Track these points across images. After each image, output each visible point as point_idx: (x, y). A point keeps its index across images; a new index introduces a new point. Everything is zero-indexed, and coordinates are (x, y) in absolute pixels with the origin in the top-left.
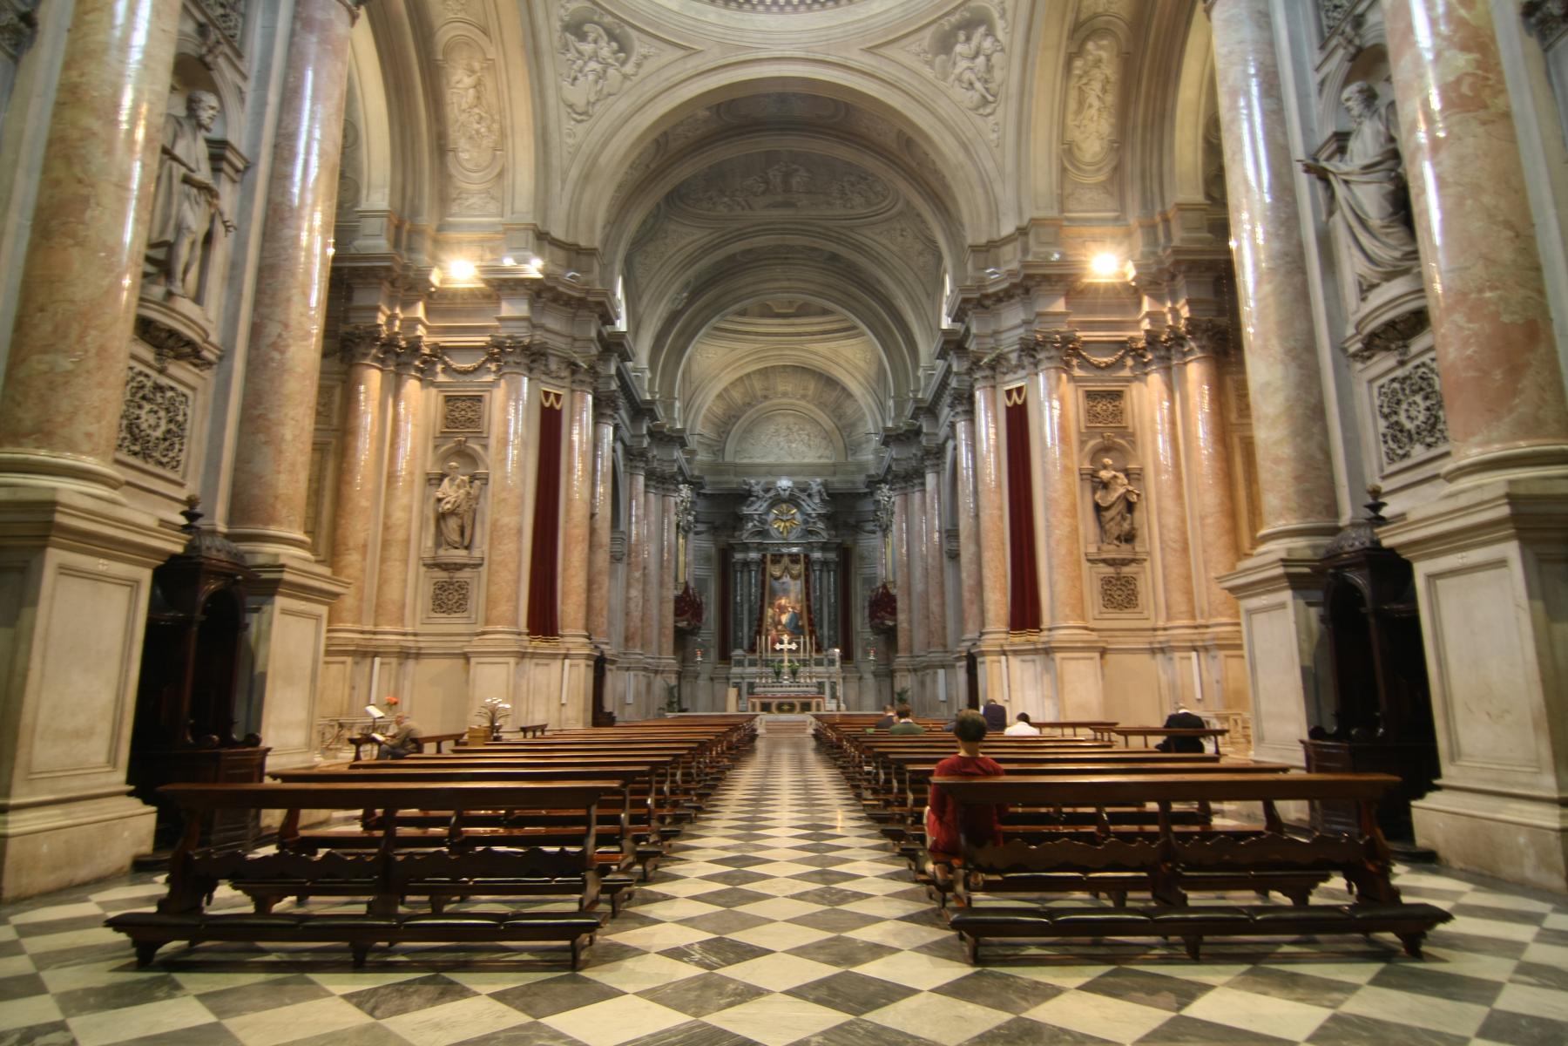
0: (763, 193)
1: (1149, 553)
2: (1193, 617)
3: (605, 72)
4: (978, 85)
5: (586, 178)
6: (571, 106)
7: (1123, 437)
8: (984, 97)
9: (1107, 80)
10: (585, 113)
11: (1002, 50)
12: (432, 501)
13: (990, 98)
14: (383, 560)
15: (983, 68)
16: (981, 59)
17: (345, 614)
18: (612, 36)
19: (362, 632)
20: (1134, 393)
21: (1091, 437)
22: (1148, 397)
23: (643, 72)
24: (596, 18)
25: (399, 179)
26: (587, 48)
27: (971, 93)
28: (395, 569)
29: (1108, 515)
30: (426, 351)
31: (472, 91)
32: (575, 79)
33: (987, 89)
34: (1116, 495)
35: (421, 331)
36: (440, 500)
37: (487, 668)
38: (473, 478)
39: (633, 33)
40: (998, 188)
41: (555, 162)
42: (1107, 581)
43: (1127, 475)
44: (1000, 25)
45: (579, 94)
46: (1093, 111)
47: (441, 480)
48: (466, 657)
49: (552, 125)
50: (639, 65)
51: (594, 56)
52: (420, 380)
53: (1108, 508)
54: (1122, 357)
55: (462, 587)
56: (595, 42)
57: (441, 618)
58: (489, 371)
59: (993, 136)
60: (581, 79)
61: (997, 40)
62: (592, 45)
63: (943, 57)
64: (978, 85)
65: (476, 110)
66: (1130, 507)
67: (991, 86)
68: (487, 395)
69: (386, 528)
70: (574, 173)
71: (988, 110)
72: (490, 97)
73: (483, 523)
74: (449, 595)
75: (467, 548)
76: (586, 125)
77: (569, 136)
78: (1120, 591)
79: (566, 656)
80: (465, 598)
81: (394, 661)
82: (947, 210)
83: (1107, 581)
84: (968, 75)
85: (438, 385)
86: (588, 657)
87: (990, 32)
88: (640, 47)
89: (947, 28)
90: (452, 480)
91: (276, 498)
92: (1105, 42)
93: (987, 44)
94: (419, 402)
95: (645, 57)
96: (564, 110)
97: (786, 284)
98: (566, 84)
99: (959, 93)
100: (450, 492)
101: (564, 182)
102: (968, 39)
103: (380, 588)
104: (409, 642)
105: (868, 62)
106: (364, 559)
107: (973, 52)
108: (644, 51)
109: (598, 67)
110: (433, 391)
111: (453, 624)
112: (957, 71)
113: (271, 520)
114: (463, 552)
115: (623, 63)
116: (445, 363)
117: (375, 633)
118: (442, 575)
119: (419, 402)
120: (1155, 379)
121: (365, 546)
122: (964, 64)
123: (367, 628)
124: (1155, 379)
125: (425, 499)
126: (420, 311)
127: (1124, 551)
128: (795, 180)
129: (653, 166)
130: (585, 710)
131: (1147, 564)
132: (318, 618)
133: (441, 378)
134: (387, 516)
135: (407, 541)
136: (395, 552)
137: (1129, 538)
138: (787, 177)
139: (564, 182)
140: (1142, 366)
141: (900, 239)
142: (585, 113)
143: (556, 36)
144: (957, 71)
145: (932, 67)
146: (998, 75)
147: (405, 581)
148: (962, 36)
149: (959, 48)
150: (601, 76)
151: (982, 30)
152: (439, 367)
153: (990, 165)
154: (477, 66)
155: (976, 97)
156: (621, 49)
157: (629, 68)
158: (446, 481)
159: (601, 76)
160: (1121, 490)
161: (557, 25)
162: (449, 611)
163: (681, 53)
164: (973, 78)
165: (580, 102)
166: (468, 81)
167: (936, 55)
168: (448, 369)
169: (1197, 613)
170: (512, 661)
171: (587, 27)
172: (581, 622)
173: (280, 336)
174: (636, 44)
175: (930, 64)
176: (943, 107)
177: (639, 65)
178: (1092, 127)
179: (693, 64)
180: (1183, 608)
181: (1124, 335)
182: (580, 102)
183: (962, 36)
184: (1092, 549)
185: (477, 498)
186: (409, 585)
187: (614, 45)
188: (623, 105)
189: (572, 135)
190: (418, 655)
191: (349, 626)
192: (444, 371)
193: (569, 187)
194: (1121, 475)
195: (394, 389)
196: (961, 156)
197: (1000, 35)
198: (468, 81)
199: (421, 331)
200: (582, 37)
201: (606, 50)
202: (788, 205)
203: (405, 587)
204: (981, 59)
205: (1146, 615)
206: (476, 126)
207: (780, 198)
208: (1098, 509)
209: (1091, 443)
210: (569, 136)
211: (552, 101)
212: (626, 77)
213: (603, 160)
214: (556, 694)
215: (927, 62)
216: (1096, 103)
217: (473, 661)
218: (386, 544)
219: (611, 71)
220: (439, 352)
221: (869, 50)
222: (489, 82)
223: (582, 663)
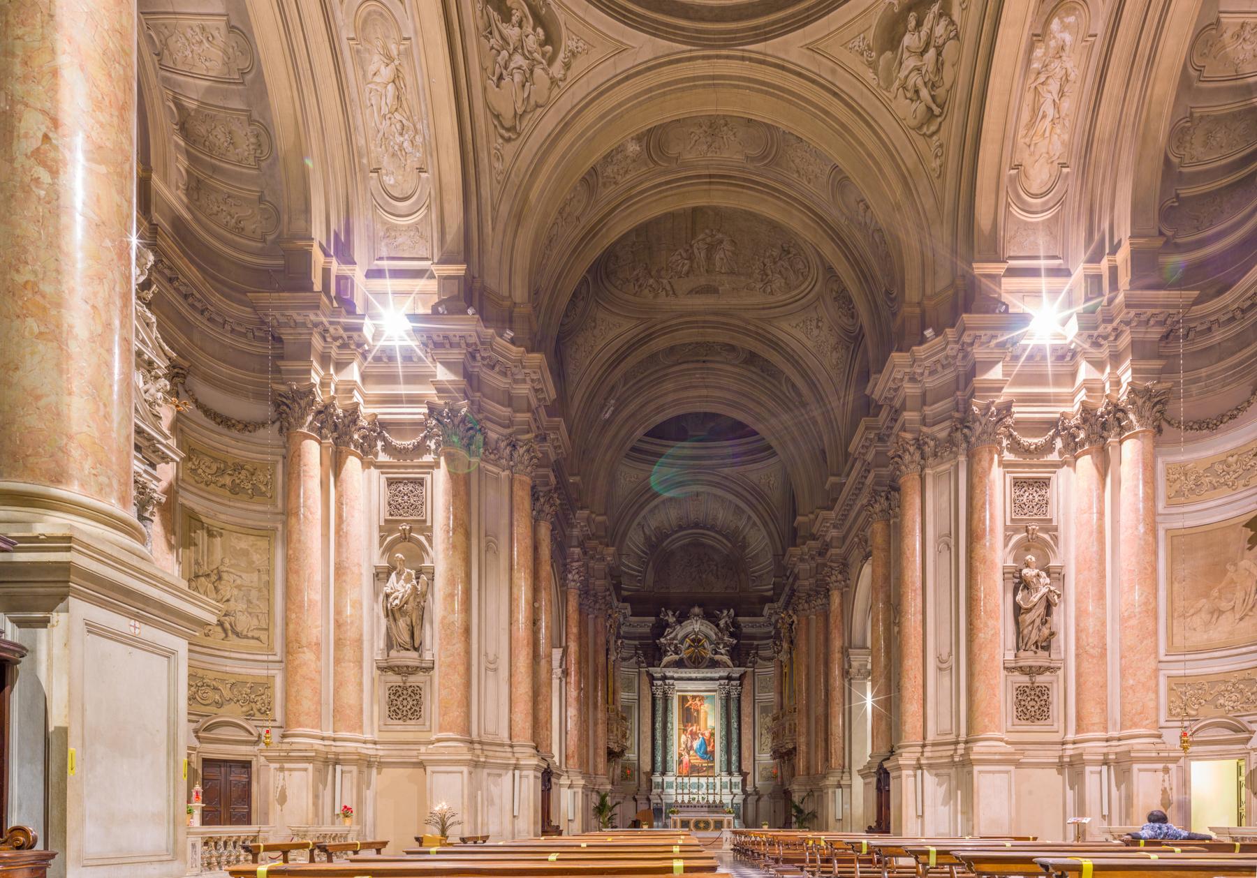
0: (687, 274)
1: (1065, 660)
2: (1106, 729)
3: (532, 72)
4: (924, 93)
5: (518, 218)
6: (497, 116)
7: (1046, 531)
8: (929, 109)
10: (512, 129)
12: (381, 597)
13: (937, 111)
14: (337, 661)
15: (931, 67)
16: (932, 52)
17: (303, 718)
18: (539, 21)
19: (323, 739)
20: (1061, 480)
21: (1016, 531)
22: (1074, 485)
26: (512, 33)
28: (349, 671)
29: (1028, 618)
30: (365, 423)
31: (391, 87)
32: (501, 78)
33: (933, 97)
34: (1039, 595)
35: (357, 398)
36: (387, 596)
37: (442, 777)
38: (419, 572)
42: (1021, 691)
43: (1049, 575)
45: (507, 99)
46: (1047, 123)
47: (389, 574)
48: (421, 765)
50: (567, 66)
52: (361, 459)
53: (1029, 610)
54: (1053, 438)
55: (416, 692)
57: (398, 725)
58: (428, 450)
59: (936, 164)
60: (507, 79)
61: (952, 22)
63: (888, 54)
64: (924, 93)
66: (1049, 606)
67: (941, 92)
68: (428, 477)
69: (338, 625)
70: (504, 209)
71: (933, 128)
73: (432, 623)
74: (404, 702)
75: (416, 649)
77: (501, 160)
78: (1033, 703)
79: (516, 767)
80: (418, 703)
81: (354, 769)
83: (1021, 691)
84: (915, 79)
85: (378, 466)
86: (536, 768)
90: (399, 574)
91: (70, 437)
94: (364, 485)
95: (574, 55)
97: (704, 392)
100: (399, 587)
102: (919, 24)
103: (336, 691)
104: (369, 750)
106: (318, 658)
108: (572, 44)
109: (524, 63)
110: (375, 472)
111: (405, 731)
113: (58, 478)
114: (414, 654)
115: (551, 61)
116: (384, 439)
117: (334, 740)
118: (396, 679)
119: (364, 485)
120: (1086, 463)
121: (318, 644)
122: (911, 62)
123: (325, 734)
124: (1086, 463)
125: (376, 595)
126: (353, 373)
127: (1041, 659)
128: (718, 256)
130: (535, 823)
131: (1061, 673)
132: (169, 654)
133: (383, 458)
134: (338, 612)
135: (360, 641)
136: (349, 652)
137: (1045, 645)
138: (711, 249)
140: (1073, 447)
141: (816, 332)
142: (512, 129)
147: (361, 684)
149: (908, 40)
150: (529, 76)
152: (380, 444)
154: (393, 49)
156: (548, 40)
157: (557, 70)
158: (393, 575)
159: (529, 76)
160: (1044, 590)
162: (404, 718)
166: (386, 73)
167: (881, 52)
168: (388, 448)
169: (1110, 727)
170: (465, 769)
172: (529, 732)
173: (46, 137)
175: (872, 65)
177: (567, 66)
178: (1042, 146)
180: (1096, 719)
181: (1052, 412)
184: (1010, 656)
185: (424, 595)
186: (368, 693)
189: (500, 158)
190: (381, 765)
191: (308, 730)
192: (385, 449)
193: (500, 227)
194: (1043, 574)
195: (336, 464)
199: (357, 398)
202: (710, 290)
203: (361, 691)
204: (932, 52)
205: (1055, 727)
206: (399, 139)
207: (703, 281)
208: (1018, 610)
209: (1016, 538)
212: (554, 81)
213: (534, 195)
214: (508, 806)
216: (1051, 112)
217: (429, 769)
218: (339, 643)
219: (538, 71)
220: (381, 427)
223: (531, 774)
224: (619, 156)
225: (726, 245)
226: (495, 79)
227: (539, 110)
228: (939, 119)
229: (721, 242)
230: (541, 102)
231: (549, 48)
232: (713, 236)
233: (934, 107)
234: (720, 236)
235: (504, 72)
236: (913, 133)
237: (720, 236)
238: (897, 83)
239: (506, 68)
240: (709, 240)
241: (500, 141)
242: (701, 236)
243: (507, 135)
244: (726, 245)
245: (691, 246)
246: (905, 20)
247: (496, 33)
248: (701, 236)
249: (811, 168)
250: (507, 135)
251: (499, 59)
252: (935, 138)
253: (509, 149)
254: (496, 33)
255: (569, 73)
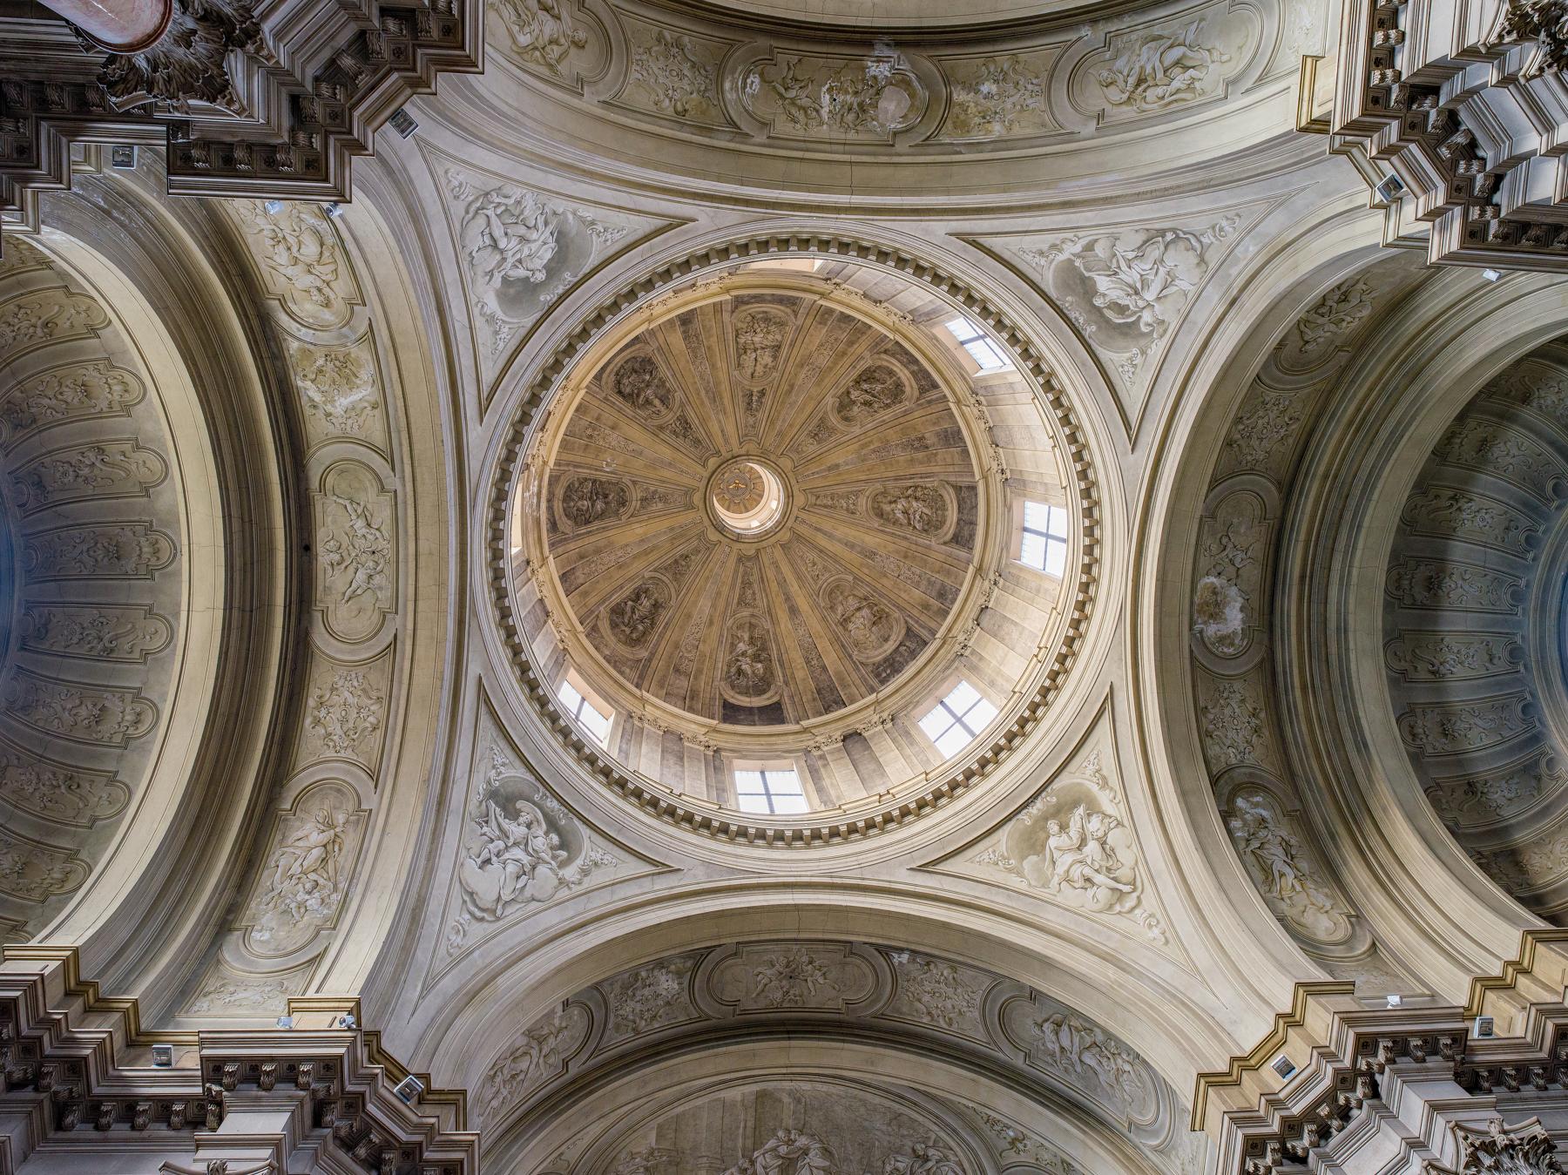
3: (534, 868)
4: (1099, 879)
9: (1287, 847)
11: (1119, 824)
13: (1126, 889)
16: (1092, 847)
18: (552, 826)
23: (588, 883)
24: (536, 798)
25: (124, 934)
26: (516, 830)
27: (1090, 892)
32: (488, 861)
33: (1115, 879)
39: (585, 831)
40: (1199, 995)
41: (422, 956)
44: (1105, 800)
45: (489, 883)
49: (434, 906)
50: (585, 873)
51: (524, 843)
56: (529, 826)
61: (1106, 816)
62: (523, 829)
63: (1033, 858)
64: (1099, 879)
65: (313, 876)
70: (449, 984)
72: (345, 859)
76: (490, 928)
82: (1102, 1122)
84: (1076, 872)
87: (1093, 809)
88: (591, 847)
89: (1029, 822)
92: (1258, 799)
93: (1095, 825)
96: (457, 896)
98: (472, 865)
99: (1070, 897)
101: (427, 989)
102: (1063, 828)
105: (925, 883)
107: (1076, 841)
109: (526, 859)
112: (1061, 869)
115: (563, 864)
122: (1069, 858)
129: (574, 1069)
139: (427, 989)
143: (474, 800)
144: (1061, 869)
145: (1020, 874)
146: (1126, 856)
148: (1053, 826)
149: (1053, 842)
151: (1081, 810)
153: (1165, 972)
154: (340, 818)
155: (1103, 895)
156: (563, 845)
157: (570, 872)
161: (480, 786)
163: (649, 869)
164: (1088, 872)
165: (487, 896)
166: (316, 838)
167: (1023, 858)
171: (520, 804)
174: (587, 843)
176: (1052, 918)
177: (585, 873)
179: (663, 886)
182: (487, 896)
183: (1053, 826)
187: (555, 839)
188: (553, 919)
193: (433, 1001)
196: (1112, 972)
197: (1109, 808)
198: (316, 838)
200: (514, 815)
201: (542, 841)
204: (1092, 847)
210: (451, 929)
211: (443, 875)
212: (562, 882)
215: (1010, 871)
219: (542, 870)
221: (922, 869)
222: (350, 841)
224: (646, 992)
225: (815, 1158)
226: (479, 861)
227: (534, 905)
228: (1135, 895)
229: (806, 1152)
230: (537, 895)
231: (564, 854)
232: (790, 1142)
233: (1120, 886)
234: (803, 1141)
235: (494, 859)
236: (1104, 917)
237: (803, 1141)
238: (1056, 880)
239: (498, 855)
240: (783, 1150)
241: (468, 916)
242: (771, 1143)
243: (479, 914)
244: (815, 1158)
245: (753, 1163)
246: (1044, 828)
247: (494, 824)
248: (771, 1143)
249: (949, 1004)
250: (479, 914)
251: (491, 846)
252: (1137, 911)
253: (478, 931)
254: (494, 824)
255: (586, 880)
